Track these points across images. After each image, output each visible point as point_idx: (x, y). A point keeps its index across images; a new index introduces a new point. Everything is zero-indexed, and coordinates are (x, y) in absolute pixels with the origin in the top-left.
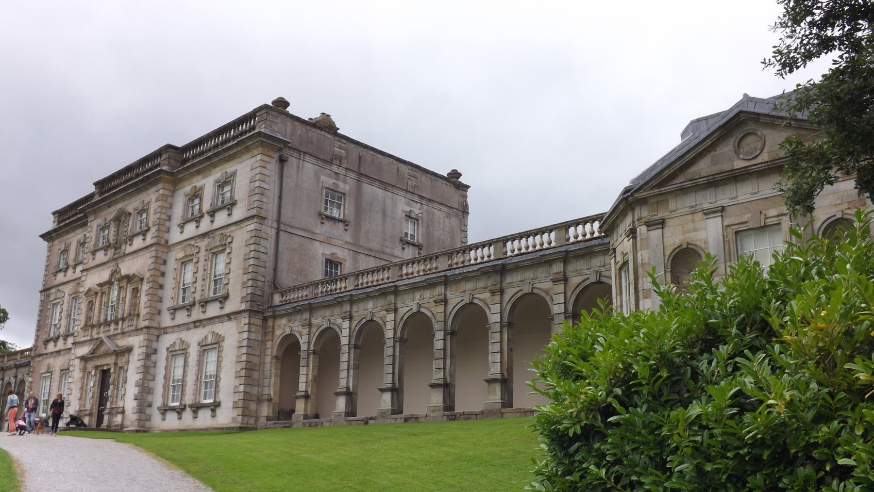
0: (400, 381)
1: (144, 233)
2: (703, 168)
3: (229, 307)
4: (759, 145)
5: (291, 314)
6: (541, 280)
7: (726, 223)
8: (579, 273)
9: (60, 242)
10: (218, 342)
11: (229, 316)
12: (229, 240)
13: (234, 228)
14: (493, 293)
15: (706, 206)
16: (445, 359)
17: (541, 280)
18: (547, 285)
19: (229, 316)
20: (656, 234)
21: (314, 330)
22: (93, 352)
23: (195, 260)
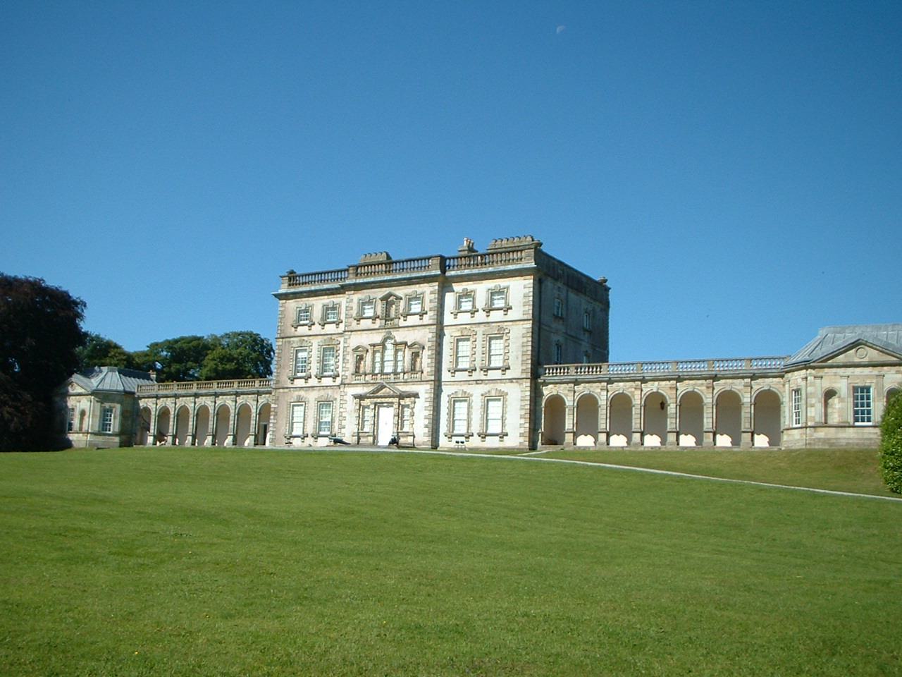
0: (196, 432)
1: (422, 315)
2: (841, 359)
3: (509, 374)
4: (865, 353)
5: (557, 383)
6: (738, 385)
7: (849, 382)
8: (759, 384)
9: (744, 397)
10: (501, 396)
11: (511, 380)
12: (507, 331)
13: (511, 323)
14: (708, 388)
15: (842, 374)
16: (676, 418)
17: (738, 385)
18: (741, 387)
19: (511, 380)
20: (818, 381)
21: (576, 394)
22: (374, 392)
23: (472, 339)
